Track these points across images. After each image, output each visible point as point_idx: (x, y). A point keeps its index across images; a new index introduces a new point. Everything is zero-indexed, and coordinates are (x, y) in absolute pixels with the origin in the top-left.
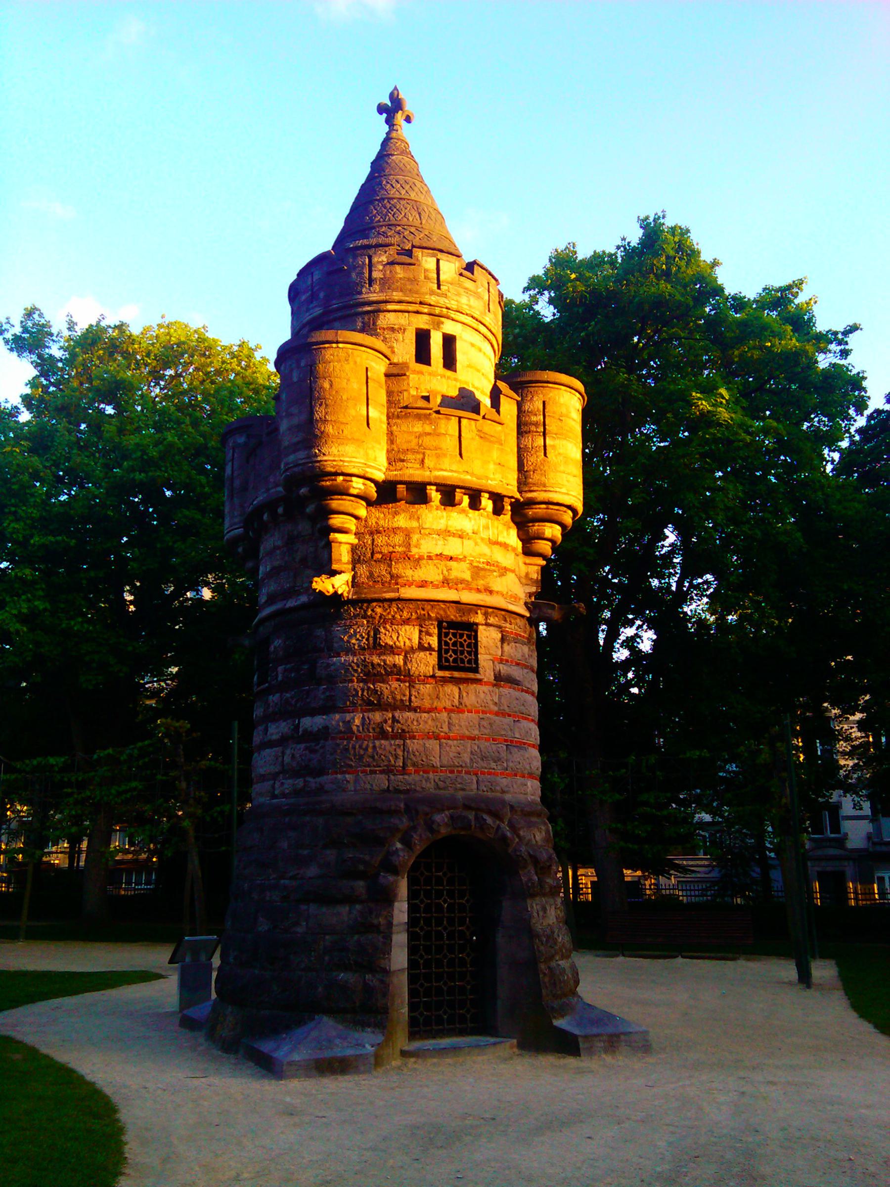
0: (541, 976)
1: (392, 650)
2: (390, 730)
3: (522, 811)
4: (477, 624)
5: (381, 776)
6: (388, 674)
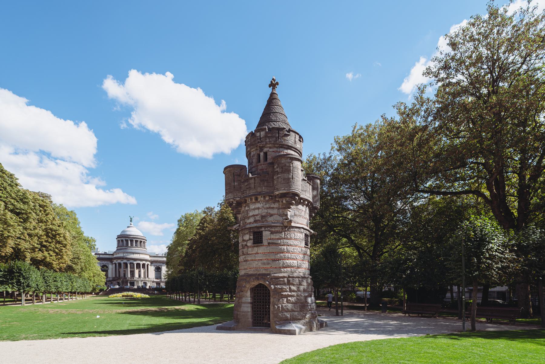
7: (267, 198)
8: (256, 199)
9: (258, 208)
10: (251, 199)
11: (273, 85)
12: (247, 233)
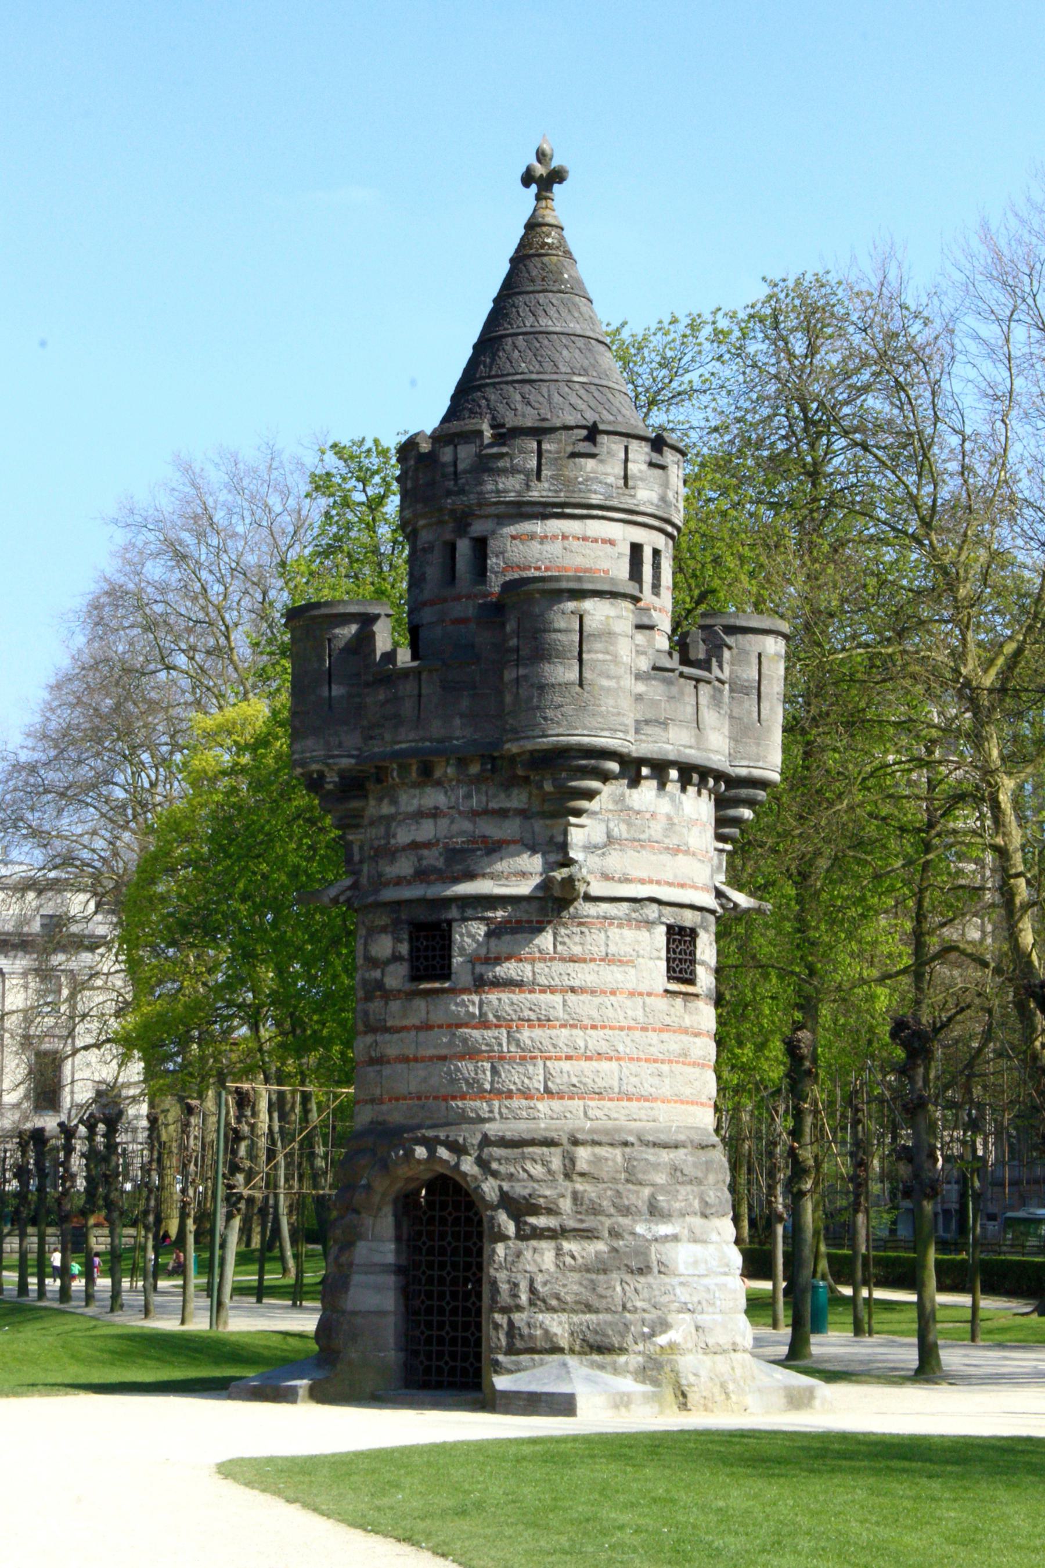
7: (474, 769)
8: (426, 771)
9: (435, 814)
10: (403, 768)
11: (544, 180)
12: (384, 929)
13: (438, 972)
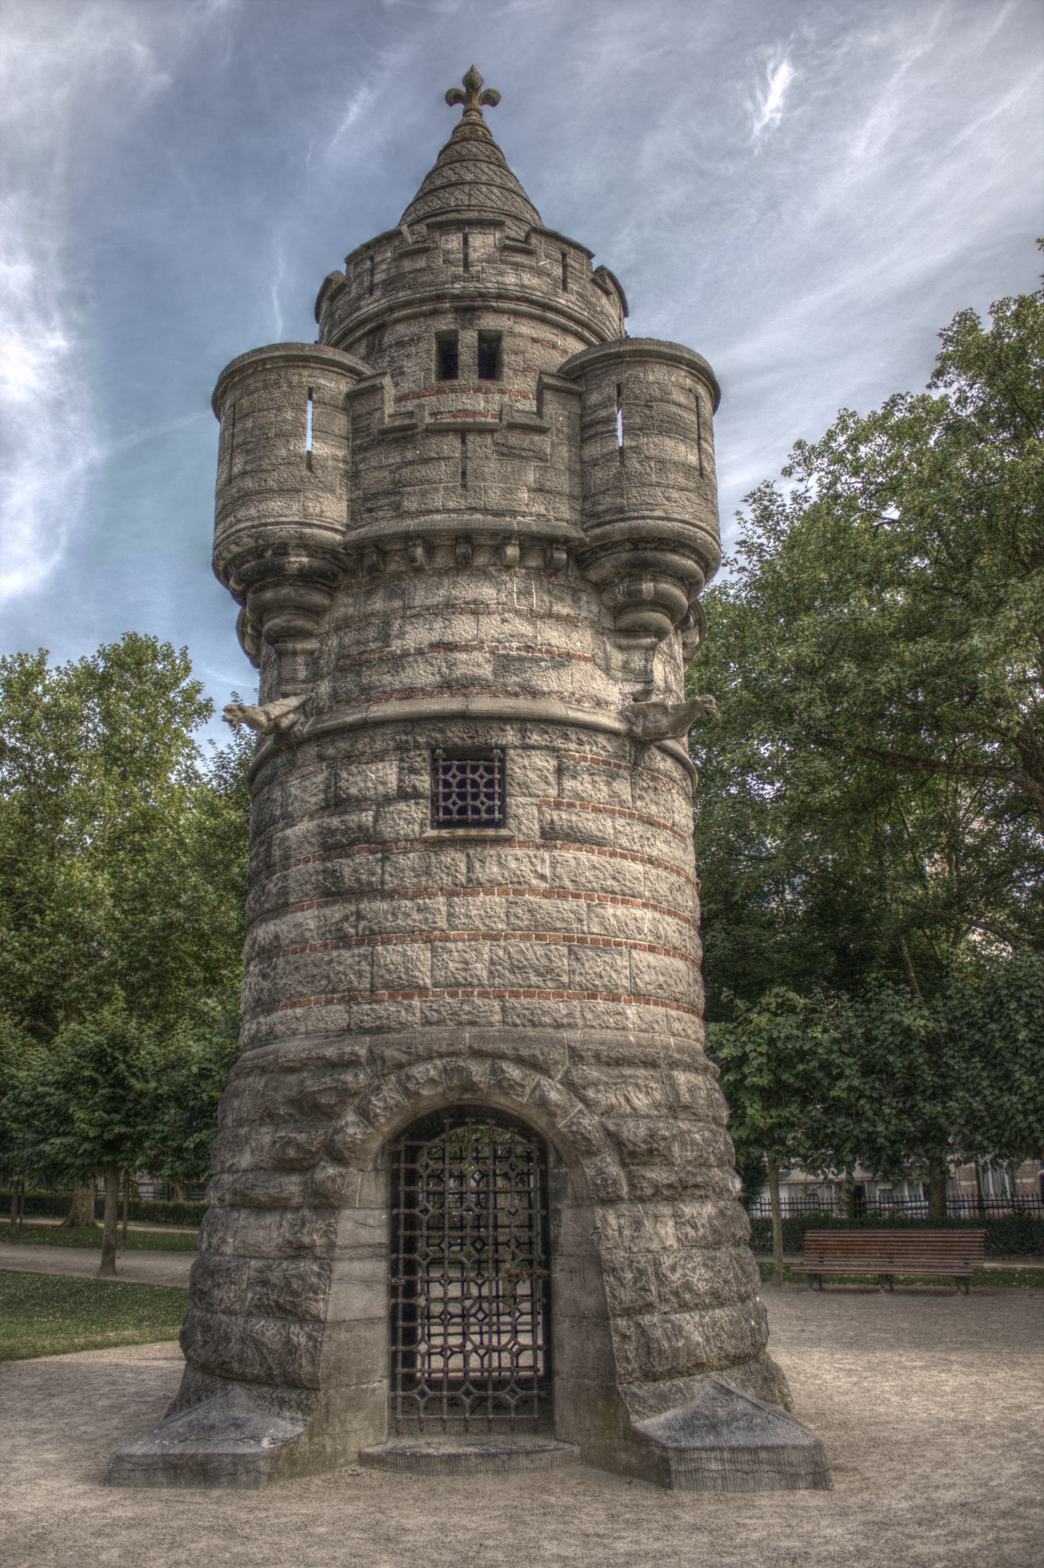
0: (616, 1339)
1: (359, 803)
2: (352, 931)
3: (597, 1056)
4: (503, 749)
5: (338, 1007)
6: (352, 843)
13: (484, 816)
